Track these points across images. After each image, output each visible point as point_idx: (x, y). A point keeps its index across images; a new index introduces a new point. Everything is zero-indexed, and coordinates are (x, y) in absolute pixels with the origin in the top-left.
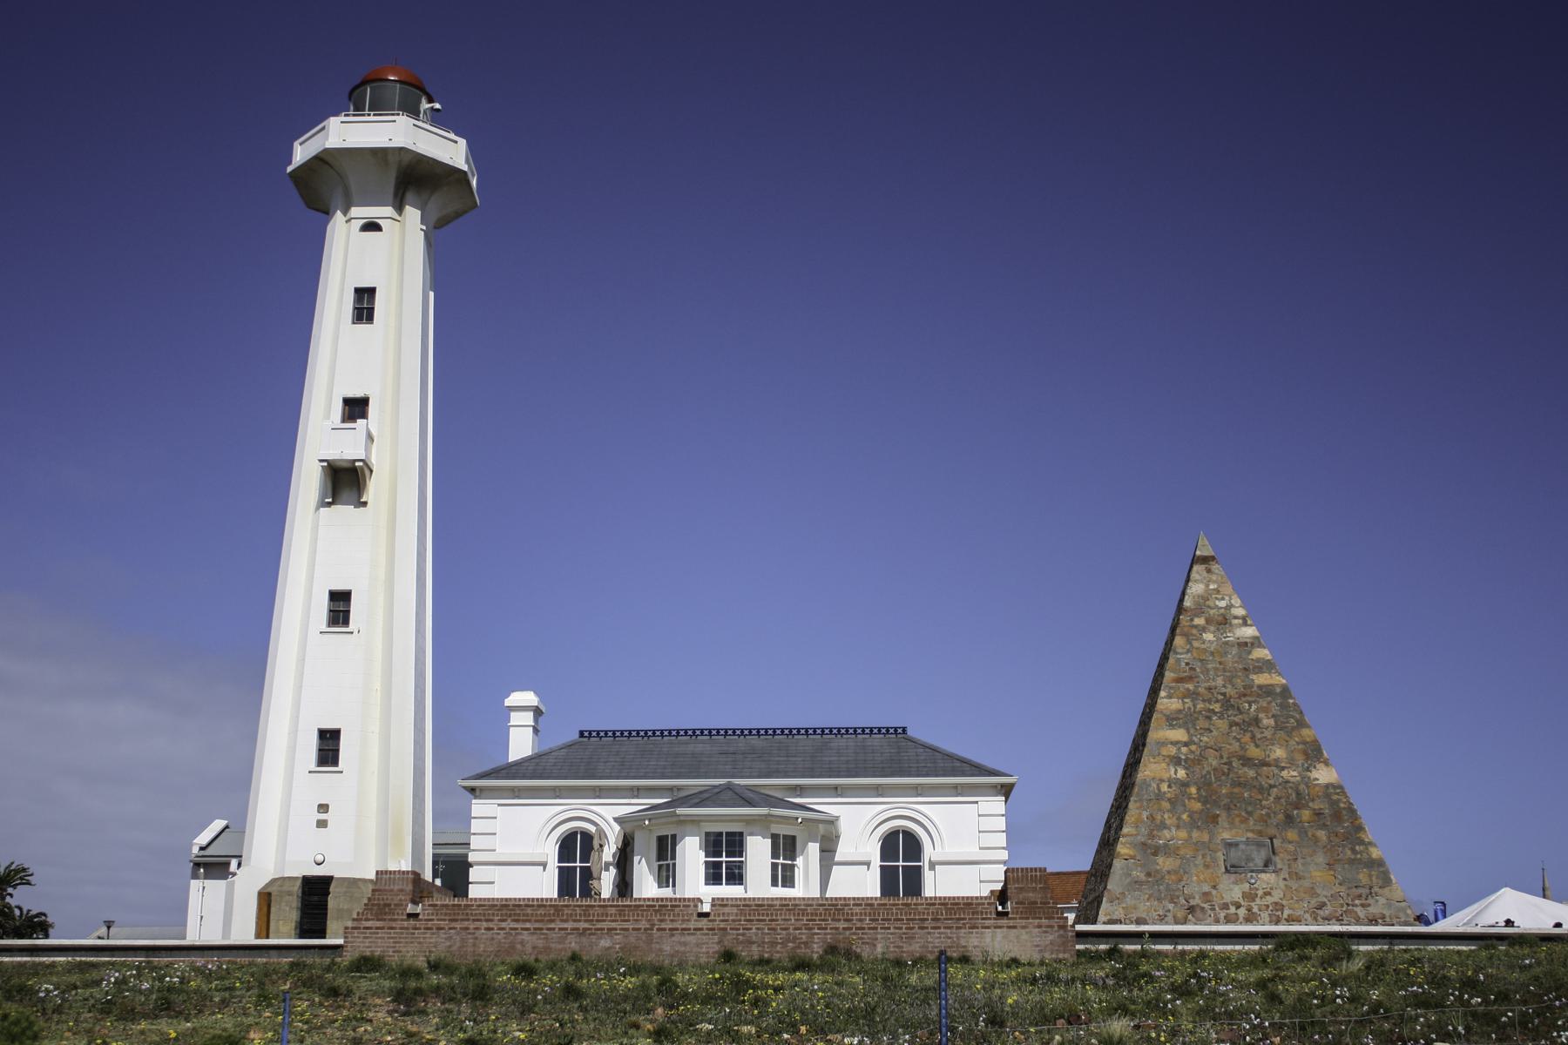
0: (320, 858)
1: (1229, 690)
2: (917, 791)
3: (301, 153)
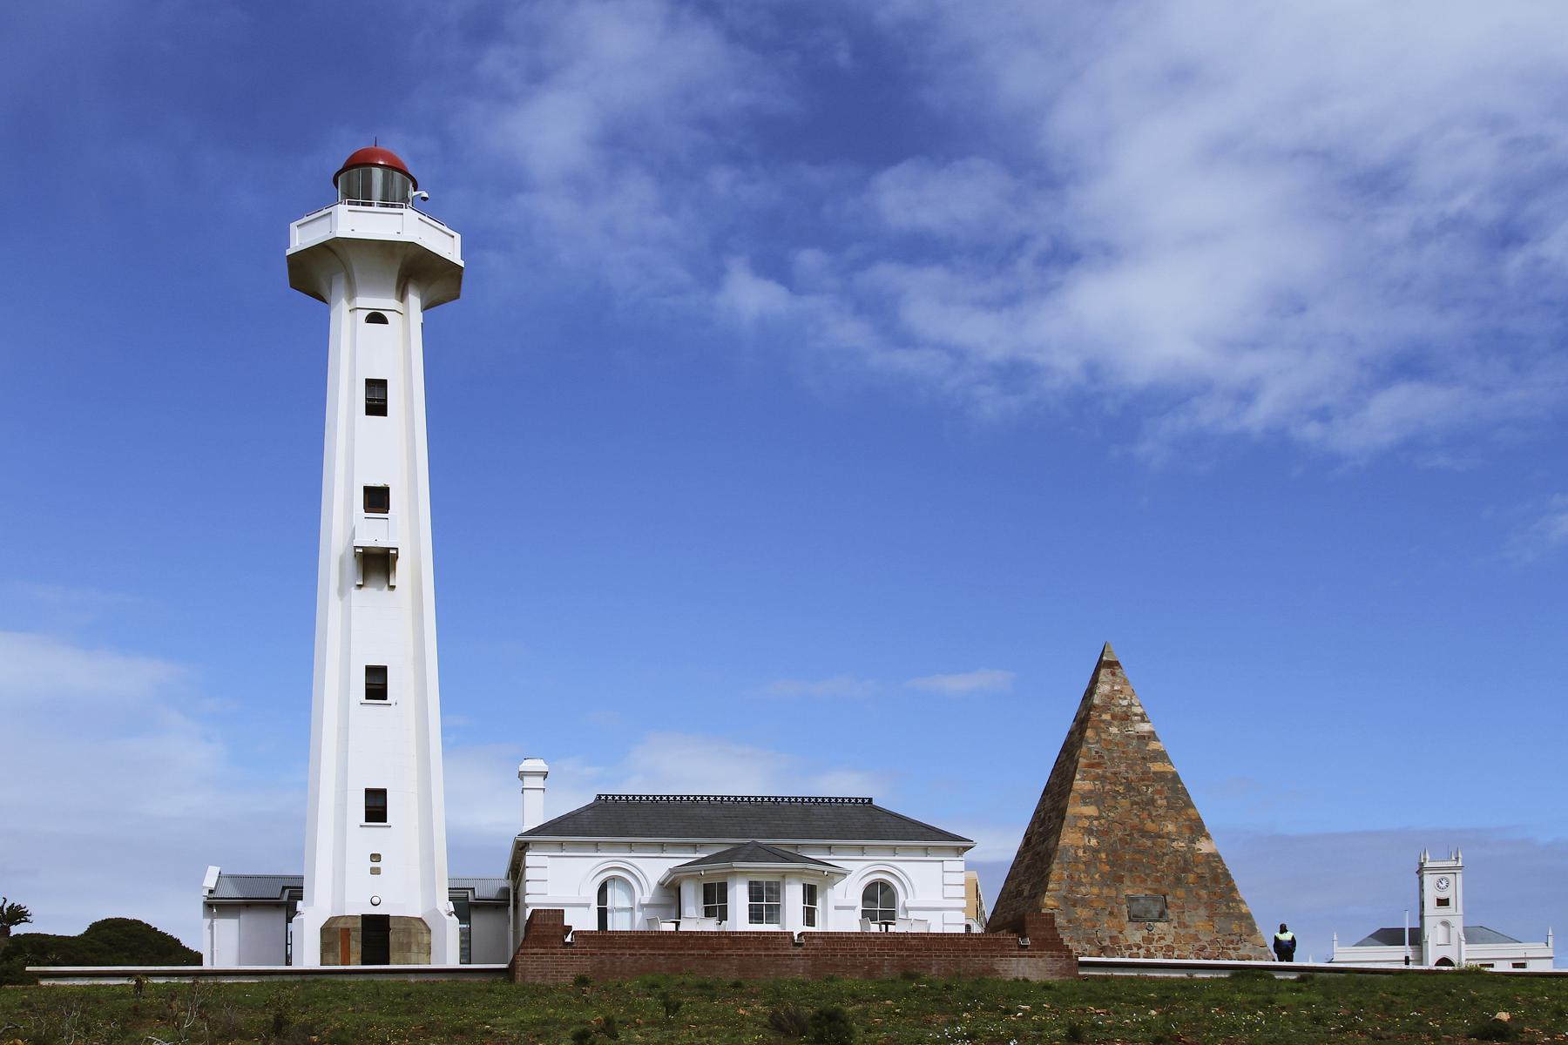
0: (376, 900)
1: (1131, 775)
2: (894, 850)
3: (302, 237)
